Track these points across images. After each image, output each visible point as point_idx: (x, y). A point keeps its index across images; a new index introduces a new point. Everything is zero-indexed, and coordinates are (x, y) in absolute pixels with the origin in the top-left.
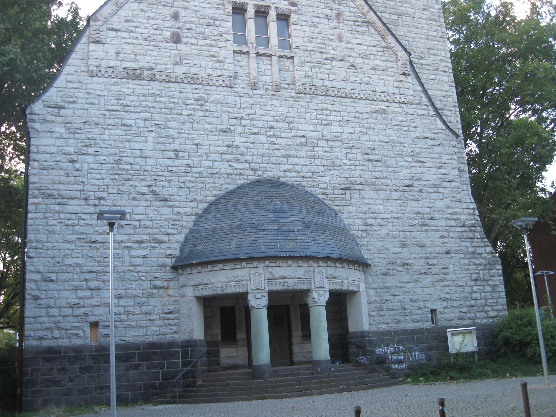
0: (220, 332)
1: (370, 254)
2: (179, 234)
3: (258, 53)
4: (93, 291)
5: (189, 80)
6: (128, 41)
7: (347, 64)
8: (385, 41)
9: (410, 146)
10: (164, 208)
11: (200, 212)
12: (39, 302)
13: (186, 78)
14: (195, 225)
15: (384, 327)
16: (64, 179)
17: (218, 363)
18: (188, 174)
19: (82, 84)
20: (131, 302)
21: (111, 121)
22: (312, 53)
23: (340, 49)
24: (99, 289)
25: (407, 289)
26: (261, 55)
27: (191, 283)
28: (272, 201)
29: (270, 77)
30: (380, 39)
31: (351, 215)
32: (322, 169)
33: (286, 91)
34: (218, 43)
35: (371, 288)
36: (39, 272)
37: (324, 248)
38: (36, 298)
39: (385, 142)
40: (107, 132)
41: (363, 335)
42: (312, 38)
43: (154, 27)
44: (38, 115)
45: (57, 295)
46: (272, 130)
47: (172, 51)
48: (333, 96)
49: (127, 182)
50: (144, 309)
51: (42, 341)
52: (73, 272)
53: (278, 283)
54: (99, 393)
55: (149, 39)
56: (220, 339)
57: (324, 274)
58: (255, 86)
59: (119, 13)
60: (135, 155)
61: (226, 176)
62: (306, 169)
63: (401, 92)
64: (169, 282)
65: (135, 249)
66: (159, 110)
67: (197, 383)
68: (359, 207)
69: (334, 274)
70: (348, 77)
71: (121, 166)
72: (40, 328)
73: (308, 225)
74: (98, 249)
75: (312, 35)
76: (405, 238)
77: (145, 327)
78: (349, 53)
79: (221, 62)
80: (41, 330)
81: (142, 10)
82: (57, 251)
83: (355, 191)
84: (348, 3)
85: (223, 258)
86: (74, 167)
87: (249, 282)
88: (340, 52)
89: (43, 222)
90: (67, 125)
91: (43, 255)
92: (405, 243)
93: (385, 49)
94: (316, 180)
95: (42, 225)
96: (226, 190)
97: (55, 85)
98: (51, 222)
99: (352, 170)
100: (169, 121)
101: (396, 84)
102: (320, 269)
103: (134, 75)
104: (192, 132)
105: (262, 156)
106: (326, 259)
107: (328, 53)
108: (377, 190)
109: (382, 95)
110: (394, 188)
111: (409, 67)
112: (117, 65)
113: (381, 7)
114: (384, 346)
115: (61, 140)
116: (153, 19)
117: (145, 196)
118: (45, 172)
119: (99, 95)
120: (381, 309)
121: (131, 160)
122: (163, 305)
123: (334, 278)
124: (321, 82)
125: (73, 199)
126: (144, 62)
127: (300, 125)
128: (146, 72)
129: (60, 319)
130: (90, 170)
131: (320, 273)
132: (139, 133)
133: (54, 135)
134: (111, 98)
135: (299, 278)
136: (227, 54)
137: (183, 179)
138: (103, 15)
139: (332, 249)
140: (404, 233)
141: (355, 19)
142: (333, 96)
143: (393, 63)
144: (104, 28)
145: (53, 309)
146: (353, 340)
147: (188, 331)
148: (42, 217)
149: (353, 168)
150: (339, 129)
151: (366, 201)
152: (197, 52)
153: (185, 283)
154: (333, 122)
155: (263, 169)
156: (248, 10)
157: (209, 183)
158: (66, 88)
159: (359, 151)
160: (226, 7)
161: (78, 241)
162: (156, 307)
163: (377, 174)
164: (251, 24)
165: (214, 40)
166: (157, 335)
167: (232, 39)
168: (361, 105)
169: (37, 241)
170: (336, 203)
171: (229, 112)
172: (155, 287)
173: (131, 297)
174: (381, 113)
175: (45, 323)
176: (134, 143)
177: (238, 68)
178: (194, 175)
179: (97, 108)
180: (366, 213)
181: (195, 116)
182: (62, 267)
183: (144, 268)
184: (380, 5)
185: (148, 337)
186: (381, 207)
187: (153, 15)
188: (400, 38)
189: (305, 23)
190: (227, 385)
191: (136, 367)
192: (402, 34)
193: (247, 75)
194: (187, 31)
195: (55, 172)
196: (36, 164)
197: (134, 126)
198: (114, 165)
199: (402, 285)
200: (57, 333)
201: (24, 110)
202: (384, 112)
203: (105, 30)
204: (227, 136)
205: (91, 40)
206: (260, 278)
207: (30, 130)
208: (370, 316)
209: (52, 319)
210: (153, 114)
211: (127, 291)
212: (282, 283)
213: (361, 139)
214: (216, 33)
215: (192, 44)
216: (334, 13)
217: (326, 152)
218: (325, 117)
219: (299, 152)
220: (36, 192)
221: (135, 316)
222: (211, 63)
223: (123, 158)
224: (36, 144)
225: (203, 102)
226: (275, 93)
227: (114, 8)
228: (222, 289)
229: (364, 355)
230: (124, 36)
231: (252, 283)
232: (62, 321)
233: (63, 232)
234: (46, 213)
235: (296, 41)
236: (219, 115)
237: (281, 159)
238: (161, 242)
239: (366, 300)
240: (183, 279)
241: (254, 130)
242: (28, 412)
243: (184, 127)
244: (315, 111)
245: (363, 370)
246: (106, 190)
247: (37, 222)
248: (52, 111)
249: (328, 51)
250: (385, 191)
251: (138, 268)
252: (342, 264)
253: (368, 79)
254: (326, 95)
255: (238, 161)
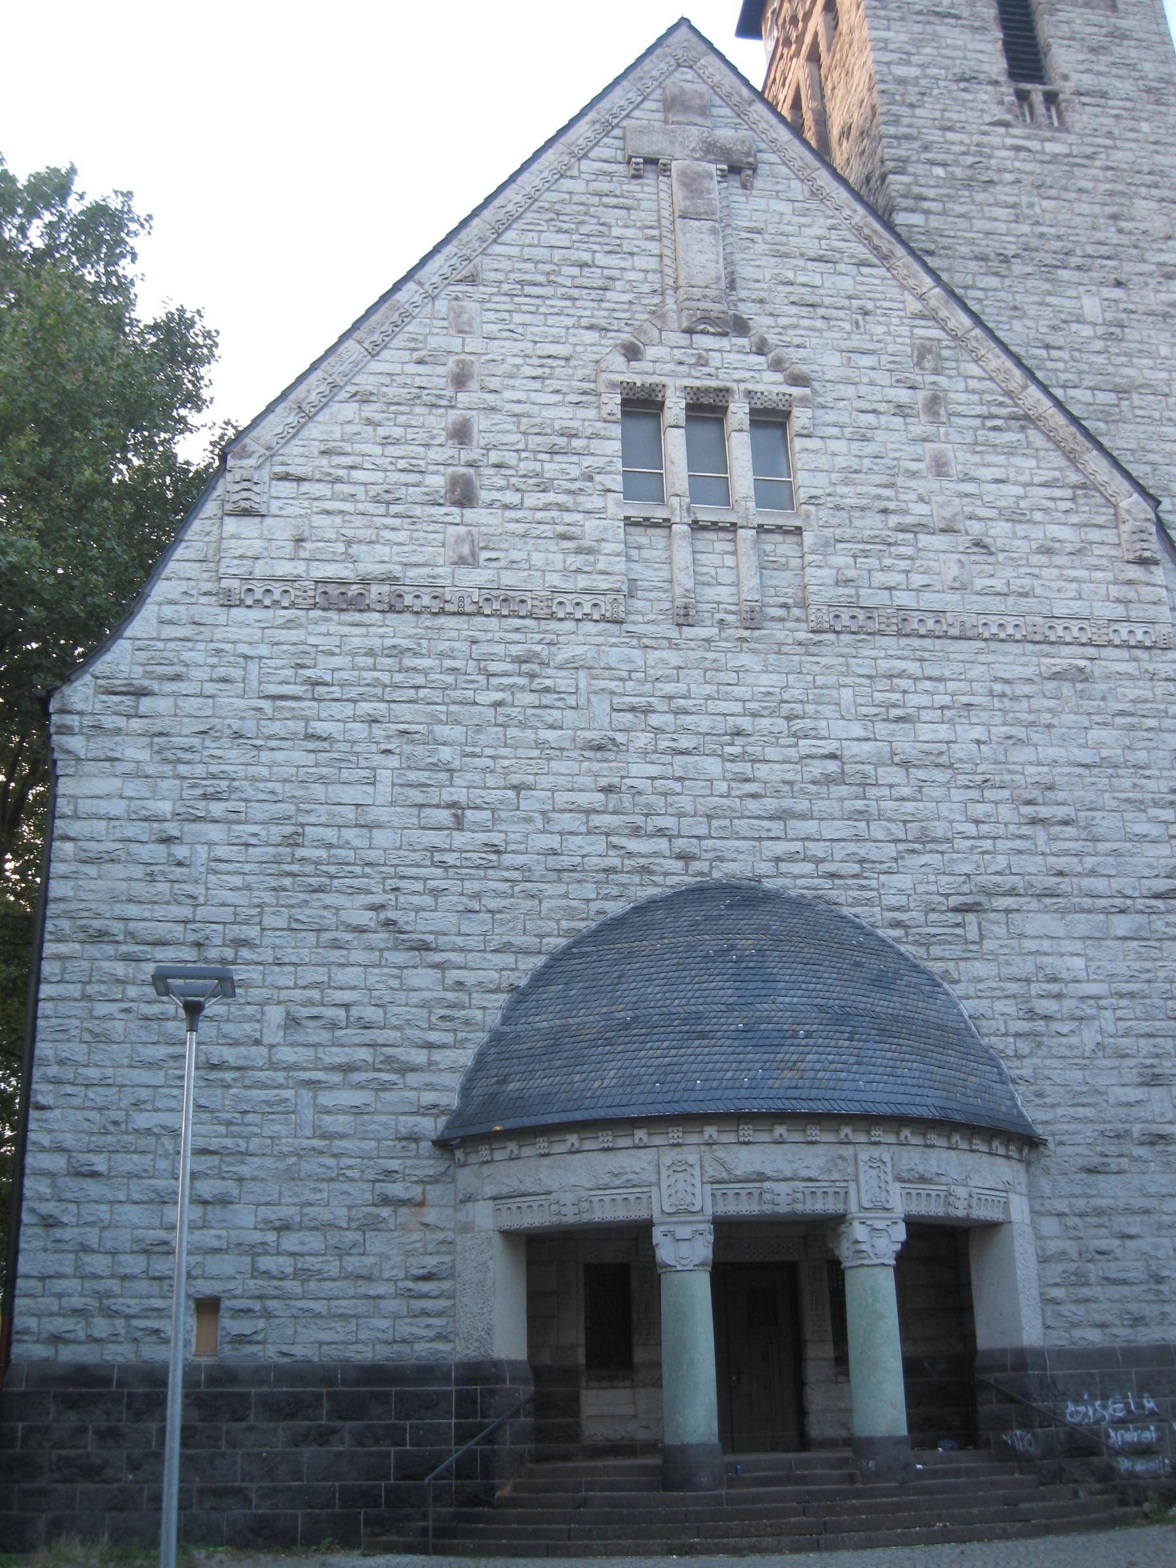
0: (582, 1340)
1: (1044, 1106)
2: (459, 1044)
3: (695, 522)
4: (209, 1208)
5: (496, 605)
6: (330, 505)
7: (964, 541)
8: (1078, 469)
9: (1166, 773)
10: (420, 971)
11: (523, 983)
12: (58, 1233)
13: (487, 600)
14: (506, 1020)
15: (1094, 1336)
16: (140, 889)
17: (572, 1433)
18: (490, 872)
19: (202, 628)
20: (315, 1242)
21: (276, 728)
22: (857, 514)
23: (941, 499)
24: (224, 1201)
25: (1165, 1218)
26: (704, 528)
27: (490, 1190)
28: (732, 948)
29: (733, 590)
30: (1063, 463)
31: (981, 987)
32: (890, 850)
33: (780, 625)
34: (581, 499)
35: (1049, 1214)
36: (61, 1150)
37: (890, 1088)
38: (49, 1223)
39: (1086, 766)
40: (265, 756)
41: (1021, 1359)
42: (856, 472)
43: (402, 464)
44: (80, 713)
45: (108, 1216)
46: (739, 740)
47: (451, 529)
48: (922, 636)
49: (315, 895)
50: (352, 1263)
51: (61, 1346)
52: (154, 1152)
53: (743, 1193)
54: (212, 1509)
55: (387, 497)
56: (582, 1360)
57: (889, 1169)
58: (686, 615)
59: (305, 433)
60: (340, 821)
61: (602, 876)
62: (840, 851)
63: (1133, 614)
64: (428, 1187)
65: (332, 1087)
66: (412, 691)
67: (498, 1494)
68: (1008, 963)
69: (921, 1168)
70: (965, 578)
71: (300, 852)
72: (55, 1308)
73: (841, 1019)
74: (229, 1087)
75: (855, 463)
76: (1157, 1056)
77: (354, 1316)
78: (967, 509)
79: (589, 551)
80: (59, 1315)
81: (369, 422)
82: (115, 1090)
83: (993, 915)
84: (963, 365)
85: (579, 1116)
86: (169, 855)
87: (654, 1189)
88: (941, 506)
89: (77, 1008)
90: (156, 740)
91: (76, 1101)
92: (1157, 1071)
93: (1079, 492)
94: (874, 883)
95: (75, 1017)
96: (601, 918)
97: (128, 633)
98: (101, 1009)
99: (983, 853)
100: (440, 722)
101: (1114, 591)
102: (876, 1152)
103: (343, 598)
104: (504, 751)
105: (708, 816)
106: (896, 1121)
107: (904, 512)
108: (1063, 912)
109: (1075, 626)
110: (1117, 902)
111: (1154, 538)
112: (295, 572)
113: (1065, 371)
114: (1093, 1397)
115: (137, 781)
116: (397, 442)
117: (365, 935)
118: (91, 870)
119: (245, 657)
120: (1082, 1280)
121: (330, 834)
122: (408, 1254)
123: (923, 1179)
124: (883, 597)
125: (164, 944)
126: (372, 560)
127: (823, 724)
128: (375, 589)
129: (114, 1285)
130: (213, 864)
131: (876, 1163)
132: (354, 759)
133: (120, 767)
134: (279, 663)
135: (810, 1180)
136: (605, 529)
137: (475, 886)
138: (262, 441)
139: (915, 1090)
140: (1152, 1041)
141: (984, 410)
142: (922, 636)
143: (1105, 531)
144: (265, 474)
145: (94, 1256)
146: (990, 1377)
147: (476, 1335)
148: (77, 995)
149: (987, 844)
150: (943, 732)
151: (1030, 945)
152: (521, 528)
153: (472, 1190)
154: (923, 712)
155: (710, 855)
156: (668, 404)
157: (550, 897)
158: (159, 640)
159: (1006, 793)
160: (604, 399)
161: (172, 1064)
162: (388, 1258)
163: (1062, 862)
164: (675, 443)
165: (569, 492)
166: (386, 1342)
167: (620, 488)
168: (1009, 659)
169: (61, 1062)
170: (936, 951)
171: (613, 693)
172: (386, 1201)
173: (316, 1229)
174: (1072, 680)
175: (70, 1295)
176: (338, 787)
177: (636, 566)
178: (506, 874)
179: (240, 692)
180: (1028, 980)
181: (513, 706)
182: (126, 1138)
183: (358, 1143)
184: (1061, 365)
185: (360, 1347)
186: (1079, 963)
187: (398, 432)
188: (1125, 459)
189: (835, 431)
190: (585, 1503)
191: (323, 1437)
192: (1133, 446)
193: (666, 585)
194: (492, 471)
195: (118, 870)
196: (68, 847)
197: (340, 738)
198: (282, 850)
199: (1150, 1203)
200: (101, 1326)
201: (45, 702)
202: (1082, 676)
203: (267, 480)
204: (605, 761)
205: (229, 507)
206: (689, 1178)
207: (56, 755)
208: (1047, 1301)
209: (89, 1285)
210: (393, 705)
211: (305, 1210)
212: (756, 1195)
213: (1010, 759)
214: (574, 472)
215: (507, 507)
216: (921, 396)
217: (903, 799)
218: (898, 696)
219: (820, 803)
220: (65, 924)
221: (327, 1285)
222: (560, 556)
223: (307, 829)
224: (71, 792)
225: (535, 667)
226: (747, 633)
227: (293, 419)
228: (575, 1209)
229: (1026, 1425)
230: (319, 494)
231: (665, 1192)
232: (117, 1290)
233: (133, 1038)
234: (89, 982)
235: (807, 483)
236: (582, 701)
237: (766, 824)
238: (407, 1069)
239: (1031, 1250)
240: (466, 1178)
241: (685, 743)
242: (7, 1552)
243: (482, 738)
244: (866, 681)
245: (1022, 1472)
246: (257, 920)
247: (63, 1008)
248: (117, 704)
249: (903, 506)
250: (1089, 911)
251: (339, 1144)
252: (949, 1138)
253: (1027, 582)
254: (900, 634)
255: (636, 832)
